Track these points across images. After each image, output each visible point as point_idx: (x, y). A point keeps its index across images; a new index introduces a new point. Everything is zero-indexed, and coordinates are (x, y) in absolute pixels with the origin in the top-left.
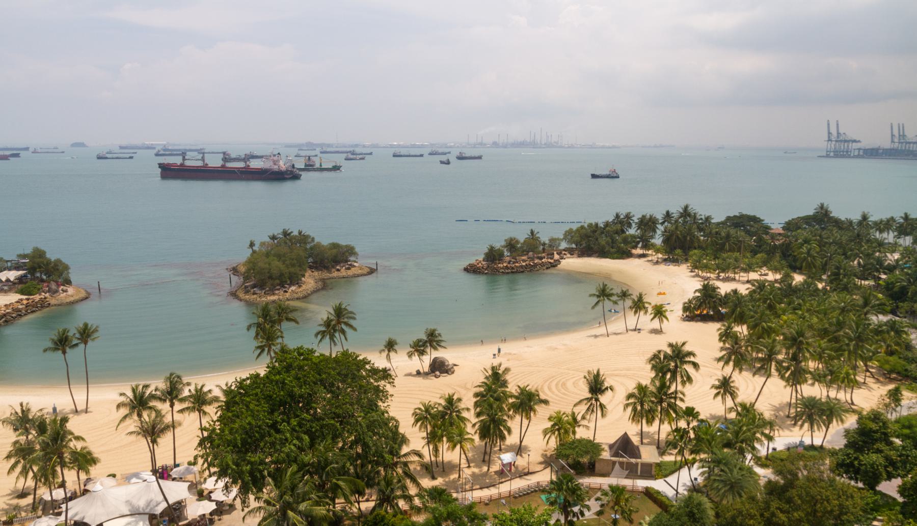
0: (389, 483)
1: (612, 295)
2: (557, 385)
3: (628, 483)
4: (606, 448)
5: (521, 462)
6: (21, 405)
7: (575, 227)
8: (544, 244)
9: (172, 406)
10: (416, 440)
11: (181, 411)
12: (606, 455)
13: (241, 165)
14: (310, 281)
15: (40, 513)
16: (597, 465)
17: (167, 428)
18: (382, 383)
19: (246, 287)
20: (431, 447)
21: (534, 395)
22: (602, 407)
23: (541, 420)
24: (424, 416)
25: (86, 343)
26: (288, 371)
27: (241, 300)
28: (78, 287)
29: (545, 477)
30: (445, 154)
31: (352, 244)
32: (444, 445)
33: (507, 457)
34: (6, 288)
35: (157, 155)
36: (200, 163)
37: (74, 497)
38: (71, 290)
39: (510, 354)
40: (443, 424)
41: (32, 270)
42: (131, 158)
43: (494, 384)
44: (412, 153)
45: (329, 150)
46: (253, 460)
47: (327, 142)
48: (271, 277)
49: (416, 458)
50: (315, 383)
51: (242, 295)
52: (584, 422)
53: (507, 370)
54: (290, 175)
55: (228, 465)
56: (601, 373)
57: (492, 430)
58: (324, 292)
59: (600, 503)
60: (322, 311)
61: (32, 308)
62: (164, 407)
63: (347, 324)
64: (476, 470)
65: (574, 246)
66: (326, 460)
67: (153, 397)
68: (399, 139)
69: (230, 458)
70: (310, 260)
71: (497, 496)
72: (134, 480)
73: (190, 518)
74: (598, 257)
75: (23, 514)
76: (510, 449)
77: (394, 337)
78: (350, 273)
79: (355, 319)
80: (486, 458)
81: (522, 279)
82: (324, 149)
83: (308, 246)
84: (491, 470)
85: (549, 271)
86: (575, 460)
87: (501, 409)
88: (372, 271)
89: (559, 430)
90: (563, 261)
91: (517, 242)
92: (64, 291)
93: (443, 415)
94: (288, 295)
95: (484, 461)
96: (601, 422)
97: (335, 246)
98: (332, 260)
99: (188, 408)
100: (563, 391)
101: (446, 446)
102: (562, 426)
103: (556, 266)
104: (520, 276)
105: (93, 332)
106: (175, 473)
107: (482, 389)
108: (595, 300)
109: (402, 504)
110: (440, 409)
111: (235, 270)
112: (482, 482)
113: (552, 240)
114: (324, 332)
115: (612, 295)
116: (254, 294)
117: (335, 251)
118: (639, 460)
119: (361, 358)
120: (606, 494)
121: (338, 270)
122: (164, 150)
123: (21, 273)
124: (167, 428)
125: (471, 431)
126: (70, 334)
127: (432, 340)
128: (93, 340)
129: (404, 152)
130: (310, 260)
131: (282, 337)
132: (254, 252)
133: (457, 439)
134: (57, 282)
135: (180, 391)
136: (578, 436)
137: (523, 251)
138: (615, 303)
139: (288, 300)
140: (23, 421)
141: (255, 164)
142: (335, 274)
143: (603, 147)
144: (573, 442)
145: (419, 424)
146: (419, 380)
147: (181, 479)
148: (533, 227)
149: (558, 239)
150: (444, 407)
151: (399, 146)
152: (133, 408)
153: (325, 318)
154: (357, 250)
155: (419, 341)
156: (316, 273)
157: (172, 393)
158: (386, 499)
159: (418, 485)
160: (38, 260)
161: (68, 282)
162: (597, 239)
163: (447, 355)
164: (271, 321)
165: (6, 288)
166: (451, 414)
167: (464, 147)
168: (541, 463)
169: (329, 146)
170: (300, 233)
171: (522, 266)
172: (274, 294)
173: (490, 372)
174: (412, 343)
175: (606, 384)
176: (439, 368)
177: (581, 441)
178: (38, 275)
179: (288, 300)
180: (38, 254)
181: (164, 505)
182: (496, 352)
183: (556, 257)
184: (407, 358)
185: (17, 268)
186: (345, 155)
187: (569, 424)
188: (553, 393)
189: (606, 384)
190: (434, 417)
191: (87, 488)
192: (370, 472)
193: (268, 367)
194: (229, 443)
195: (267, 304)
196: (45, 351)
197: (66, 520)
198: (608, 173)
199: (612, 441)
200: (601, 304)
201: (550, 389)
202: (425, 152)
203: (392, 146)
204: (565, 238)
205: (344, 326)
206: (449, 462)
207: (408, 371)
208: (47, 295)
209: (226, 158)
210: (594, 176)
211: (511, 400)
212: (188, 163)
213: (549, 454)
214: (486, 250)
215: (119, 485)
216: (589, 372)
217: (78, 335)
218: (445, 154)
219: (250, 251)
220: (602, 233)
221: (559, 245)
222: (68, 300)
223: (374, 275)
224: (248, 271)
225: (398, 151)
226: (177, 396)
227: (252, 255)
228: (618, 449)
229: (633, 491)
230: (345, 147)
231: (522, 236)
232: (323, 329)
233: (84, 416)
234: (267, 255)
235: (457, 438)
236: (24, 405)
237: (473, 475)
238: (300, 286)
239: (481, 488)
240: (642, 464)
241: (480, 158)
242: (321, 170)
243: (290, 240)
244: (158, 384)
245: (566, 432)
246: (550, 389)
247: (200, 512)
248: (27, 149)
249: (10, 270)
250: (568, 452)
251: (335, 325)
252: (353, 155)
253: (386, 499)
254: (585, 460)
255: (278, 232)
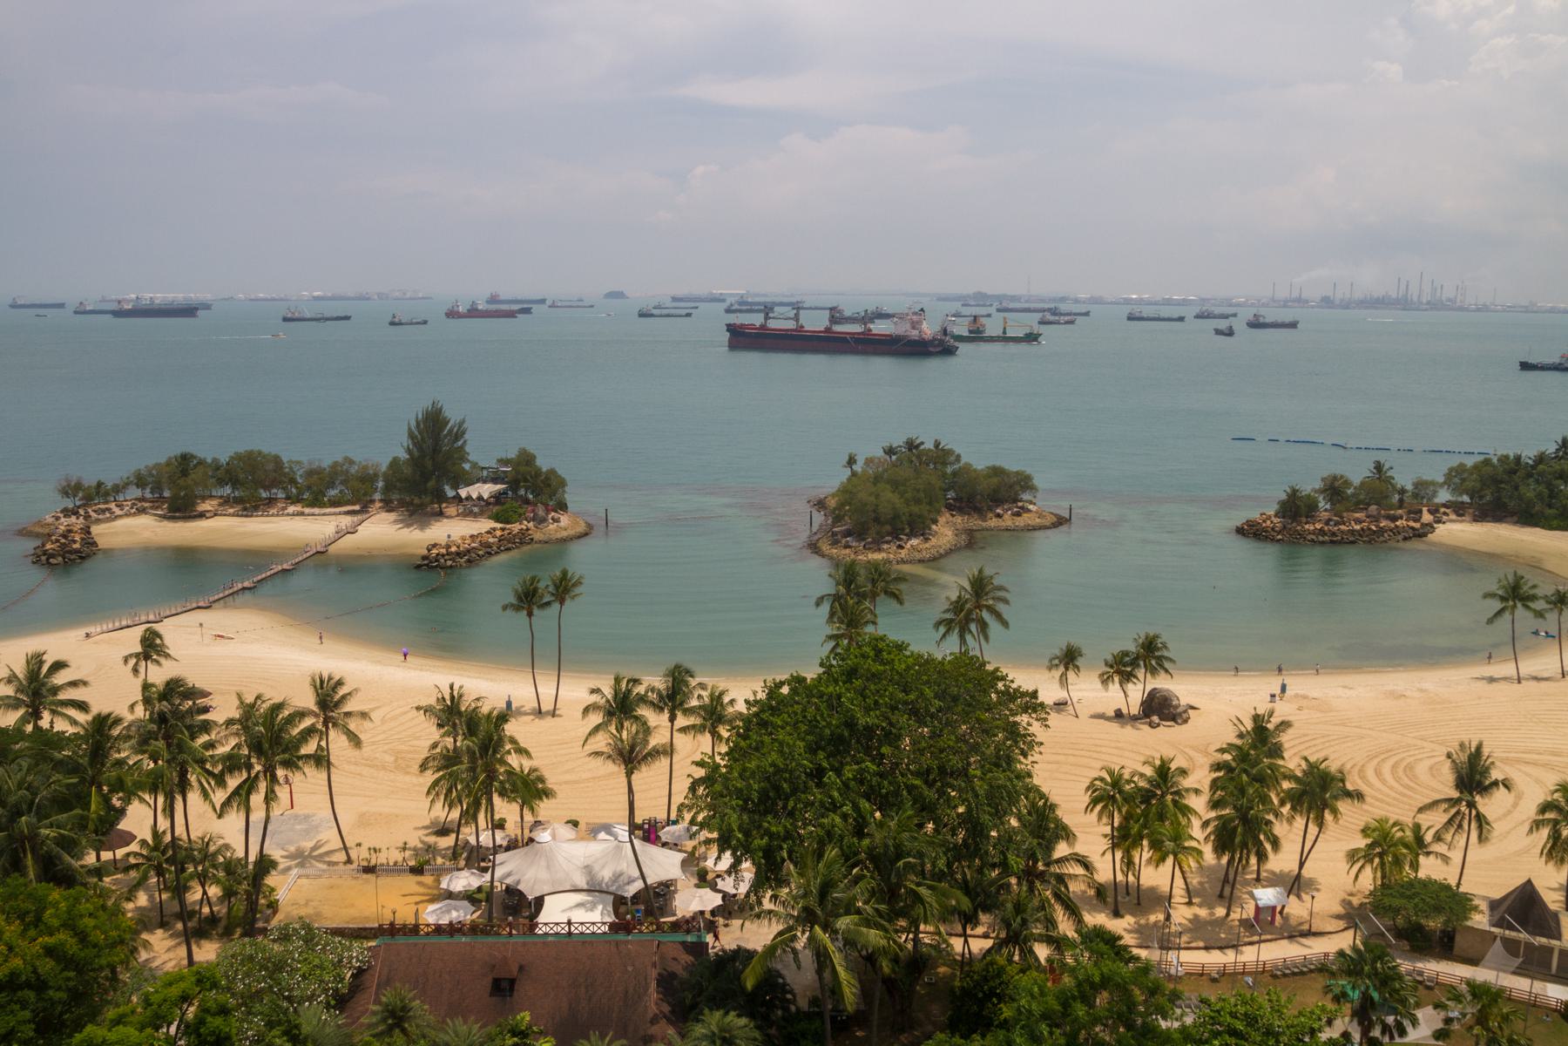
0: (1019, 908)
1: (1534, 598)
2: (1394, 767)
3: (1520, 985)
4: (1484, 906)
5: (1297, 909)
6: (451, 687)
7: (1470, 462)
8: (1402, 491)
9: (672, 719)
10: (1090, 839)
11: (684, 730)
12: (1480, 920)
13: (856, 328)
14: (945, 531)
15: (462, 863)
16: (1458, 938)
17: (656, 753)
18: (1023, 719)
19: (834, 534)
20: (1119, 855)
21: (1333, 779)
22: (1481, 820)
23: (1344, 832)
24: (1109, 794)
25: (562, 602)
26: (849, 681)
27: (823, 556)
28: (577, 515)
29: (1345, 941)
30: (1226, 317)
31: (1028, 471)
32: (1144, 854)
33: (1267, 896)
34: (476, 509)
35: (728, 311)
36: (791, 325)
37: (512, 846)
38: (565, 520)
39: (1305, 697)
40: (1145, 814)
41: (514, 484)
42: (688, 315)
43: (1254, 747)
44: (1163, 315)
45: (1011, 306)
46: (774, 829)
47: (1010, 293)
48: (877, 520)
49: (1080, 870)
50: (894, 708)
51: (825, 548)
52: (1440, 848)
53: (1285, 725)
54: (940, 347)
55: (731, 831)
56: (1486, 751)
57: (1241, 835)
58: (969, 553)
59: (1443, 1014)
60: (953, 584)
61: (508, 543)
62: (657, 720)
63: (992, 610)
64: (1203, 913)
65: (1466, 498)
66: (898, 847)
67: (642, 699)
68: (1140, 289)
69: (734, 818)
70: (951, 494)
71: (1240, 968)
72: (602, 835)
73: (680, 914)
74: (1515, 523)
75: (439, 860)
76: (1274, 880)
77: (1076, 642)
78: (1020, 522)
79: (1006, 602)
80: (1226, 889)
81: (1351, 555)
82: (1005, 305)
83: (949, 470)
84: (1233, 916)
85: (1408, 545)
86: (1411, 916)
87: (1265, 799)
88: (1060, 522)
89: (1381, 855)
90: (1440, 528)
91: (1347, 483)
92: (555, 520)
93: (1146, 796)
94: (903, 553)
95: (1221, 896)
96: (1476, 852)
97: (997, 471)
98: (990, 496)
99: (694, 726)
100: (1406, 780)
101: (1146, 855)
102: (1387, 847)
103: (1425, 535)
104: (1351, 549)
105: (574, 585)
106: (666, 834)
107: (1227, 757)
108: (1498, 605)
109: (1042, 952)
110: (1142, 784)
111: (820, 504)
112: (1208, 935)
113: (1420, 485)
114: (951, 621)
115: (1534, 598)
116: (847, 547)
117: (995, 480)
118: (1555, 942)
119: (989, 668)
120: (1458, 998)
121: (999, 516)
122: (740, 304)
123: (499, 487)
124: (656, 753)
125: (1198, 834)
126: (541, 585)
127: (1150, 655)
128: (573, 598)
129: (1147, 311)
130: (951, 494)
131: (874, 623)
132: (854, 474)
133: (1170, 846)
134: (546, 505)
135: (687, 696)
136: (1422, 874)
137: (1358, 503)
138: (1540, 614)
139: (903, 562)
140: (451, 713)
141: (880, 328)
142: (993, 522)
143: (1552, 311)
144: (1411, 884)
145: (1099, 807)
146: (1114, 727)
147: (675, 846)
148: (1381, 457)
149: (1433, 483)
150: (1150, 781)
151: (1140, 302)
152: (610, 714)
153: (954, 598)
154: (1036, 482)
155: (1125, 654)
156: (958, 519)
157: (673, 699)
158: (1015, 937)
159: (1079, 921)
160: (523, 469)
161: (562, 507)
162: (1516, 488)
163: (1181, 687)
164: (858, 594)
165: (476, 509)
166: (1163, 796)
167: (1264, 305)
168: (1338, 917)
169: (1013, 298)
170: (937, 444)
171: (1352, 532)
172: (879, 550)
173: (1249, 725)
174: (1110, 658)
175: (1495, 774)
176: (1159, 709)
177: (1427, 884)
178: (522, 492)
179: (903, 562)
180: (526, 459)
181: (639, 885)
182: (1277, 691)
183: (1427, 517)
184: (1099, 685)
185: (495, 481)
186: (1039, 315)
187: (1406, 846)
188: (1384, 782)
189: (1495, 774)
190: (1128, 798)
191: (533, 835)
192: (993, 882)
193: (821, 665)
194: (739, 792)
195: (853, 562)
196: (505, 608)
197: (492, 881)
198: (1557, 361)
199: (1497, 895)
200: (1507, 616)
201: (1378, 773)
202: (1190, 313)
203: (1128, 301)
204: (1448, 481)
205: (986, 615)
206: (1153, 890)
207: (1100, 710)
208: (531, 525)
209: (836, 315)
210: (1525, 366)
211: (1286, 785)
212: (772, 324)
213: (1356, 901)
214: (1284, 497)
215: (579, 839)
216: (1462, 745)
217: (551, 589)
218: (1226, 317)
219: (848, 472)
220: (1530, 475)
221: (1435, 494)
222: (559, 536)
223: (1064, 528)
224: (841, 505)
225: (1136, 310)
226: (681, 704)
227: (849, 480)
228: (1510, 911)
229: (1533, 1006)
230: (1043, 301)
231: (1357, 472)
232: (949, 616)
233: (549, 719)
234: (877, 479)
235: (1169, 844)
236: (456, 687)
237: (1196, 919)
238: (927, 540)
239: (1206, 948)
240: (1562, 952)
241: (1293, 325)
242: (1005, 339)
243: (919, 457)
244: (654, 681)
245: (1398, 862)
246: (1378, 773)
247: (695, 907)
248: (543, 301)
249: (485, 482)
250: (1397, 902)
251: (970, 612)
252: (1054, 315)
253: (1015, 937)
254: (1434, 924)
255: (898, 441)
